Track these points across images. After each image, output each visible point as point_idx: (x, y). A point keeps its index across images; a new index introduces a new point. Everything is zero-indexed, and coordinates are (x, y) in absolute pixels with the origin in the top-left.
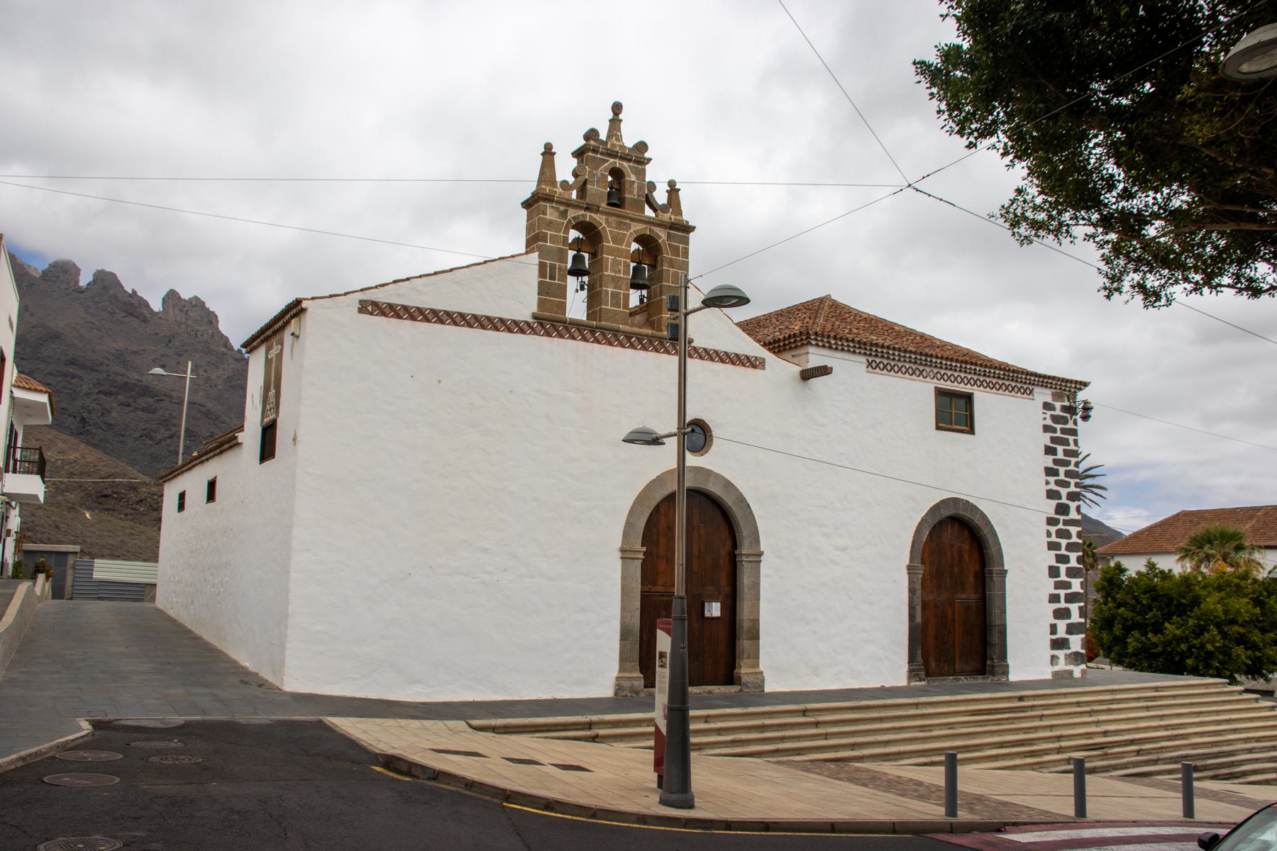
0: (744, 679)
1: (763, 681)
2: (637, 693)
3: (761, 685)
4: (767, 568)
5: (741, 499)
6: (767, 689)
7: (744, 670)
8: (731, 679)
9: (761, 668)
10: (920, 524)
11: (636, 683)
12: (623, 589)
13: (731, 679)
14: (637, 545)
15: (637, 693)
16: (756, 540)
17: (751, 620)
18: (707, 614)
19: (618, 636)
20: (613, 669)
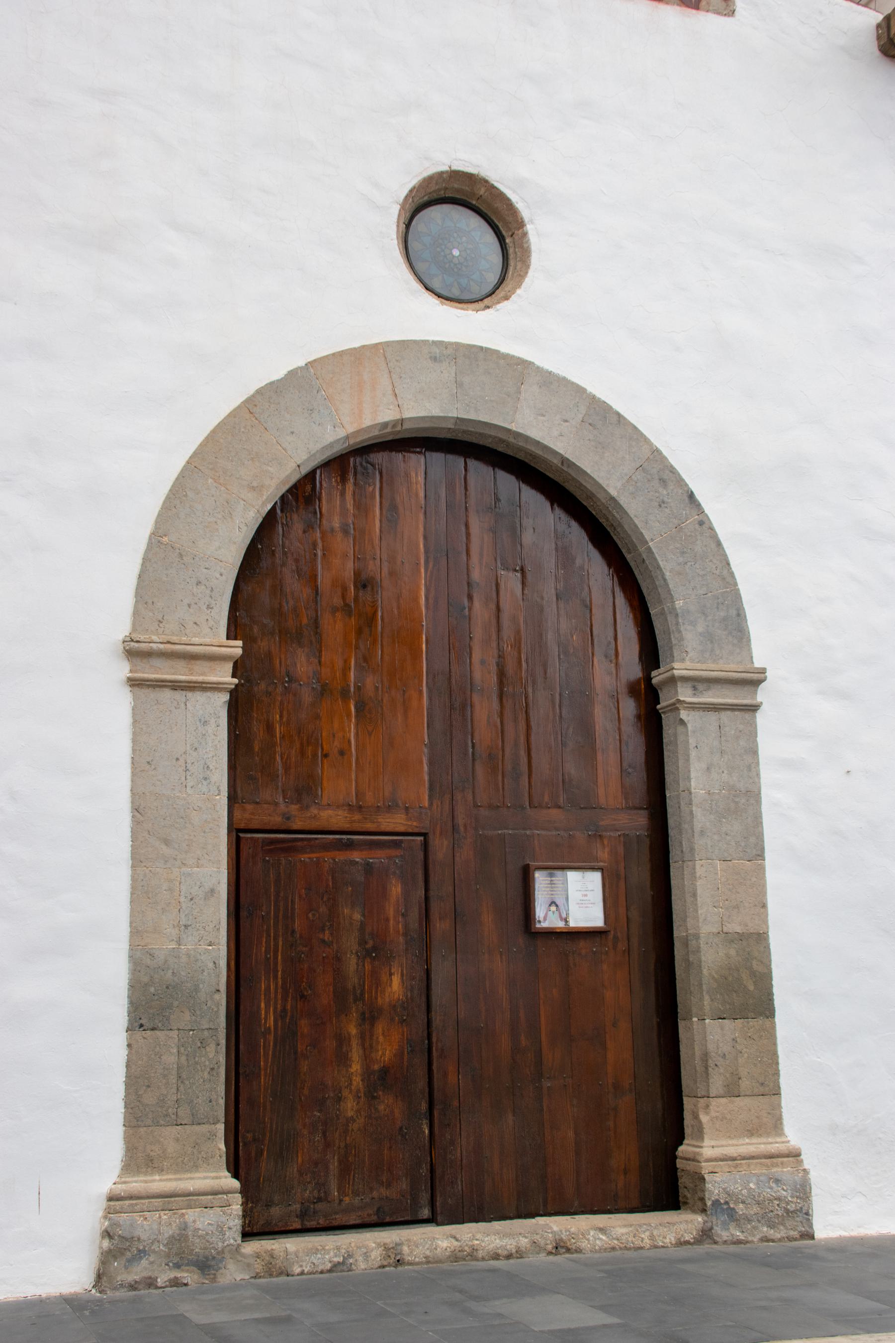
0: (717, 1184)
1: (803, 1191)
2: (206, 1265)
3: (798, 1210)
4: (782, 733)
5: (660, 473)
6: (829, 1224)
7: (714, 1146)
8: (665, 1186)
9: (793, 1134)
10: (356, 358)
11: (201, 1220)
12: (137, 810)
13: (665, 1186)
14: (208, 627)
15: (206, 1265)
16: (736, 628)
17: (731, 938)
18: (545, 917)
19: (116, 1012)
20: (93, 1158)
